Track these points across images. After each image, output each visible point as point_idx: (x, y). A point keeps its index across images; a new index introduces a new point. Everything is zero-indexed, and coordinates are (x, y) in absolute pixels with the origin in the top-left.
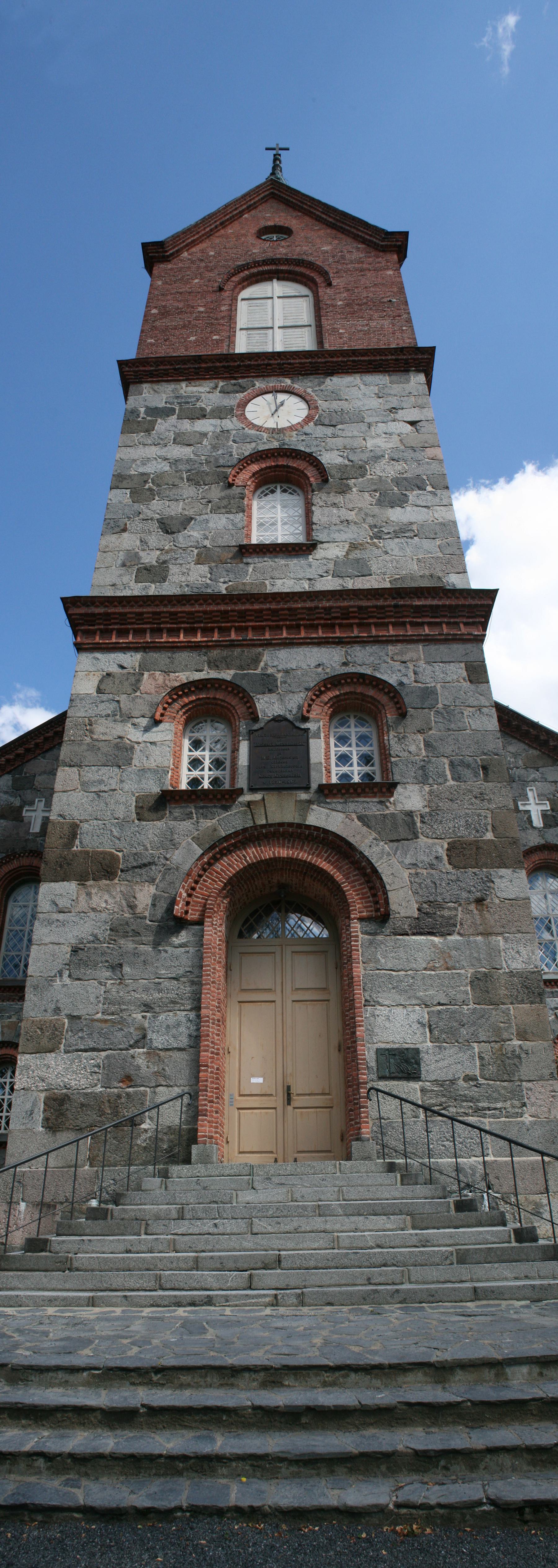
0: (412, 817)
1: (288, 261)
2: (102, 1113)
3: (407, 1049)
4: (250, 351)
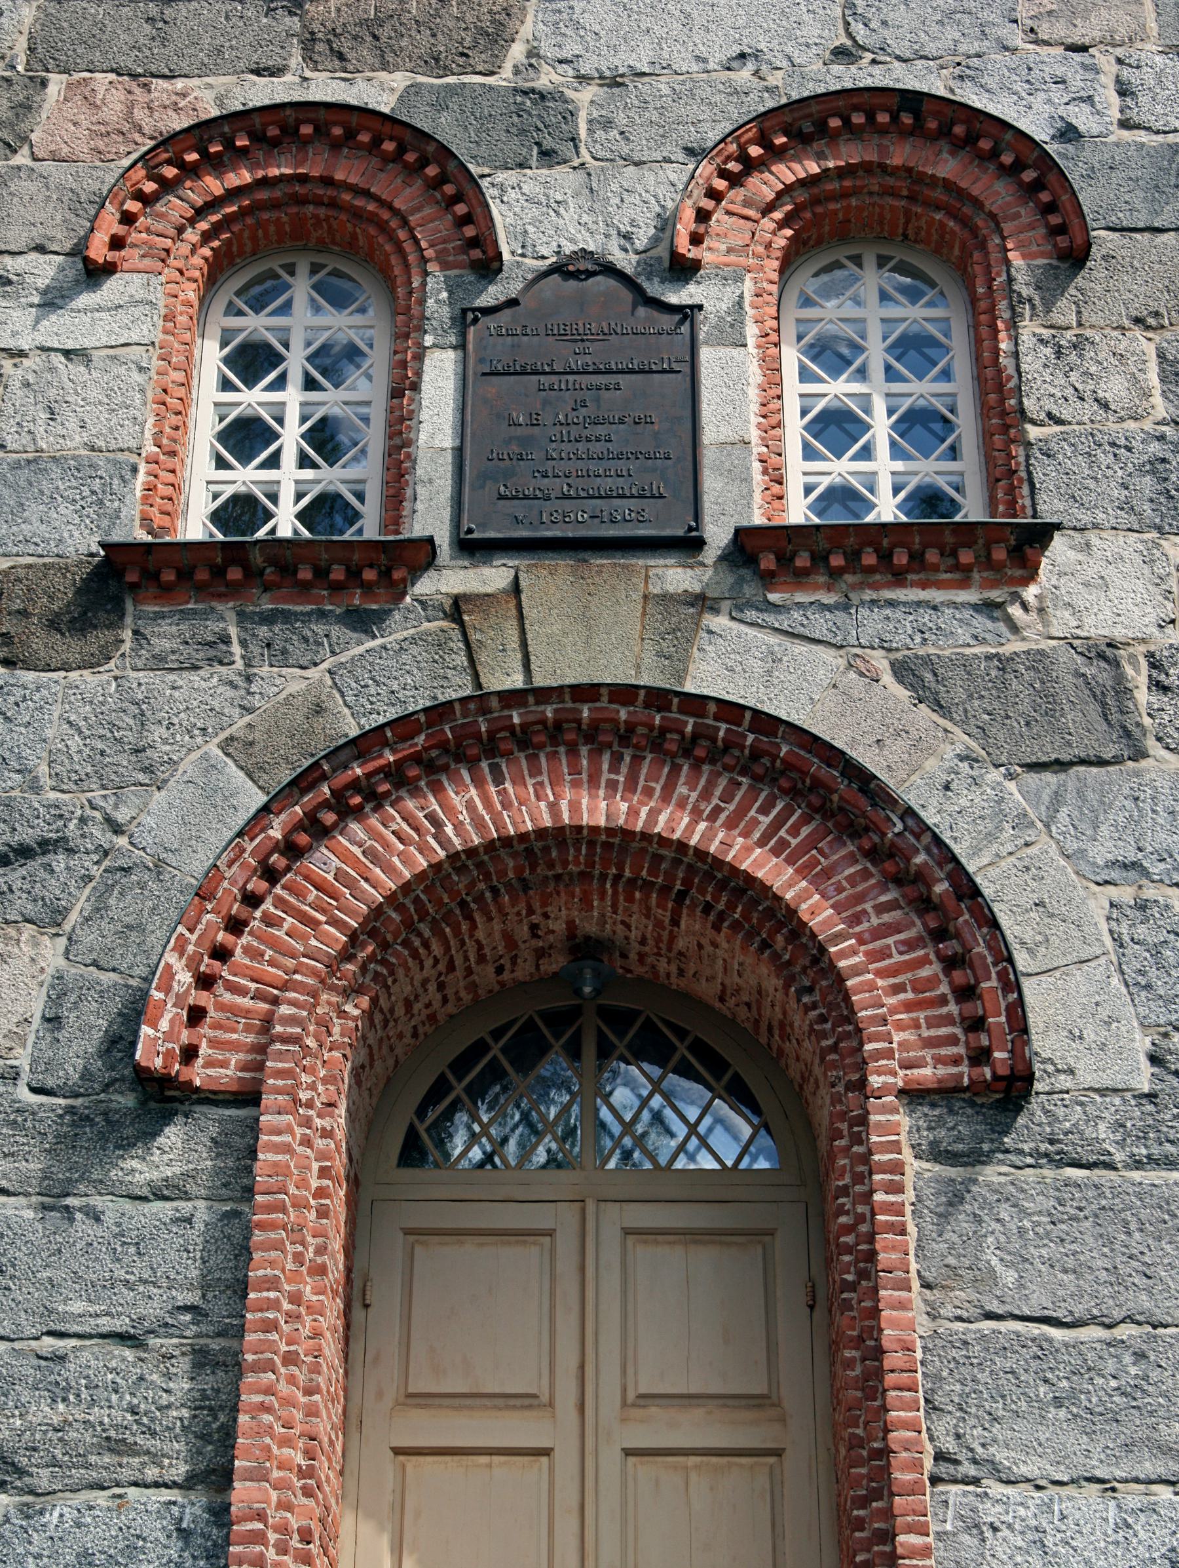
0: (1115, 663)
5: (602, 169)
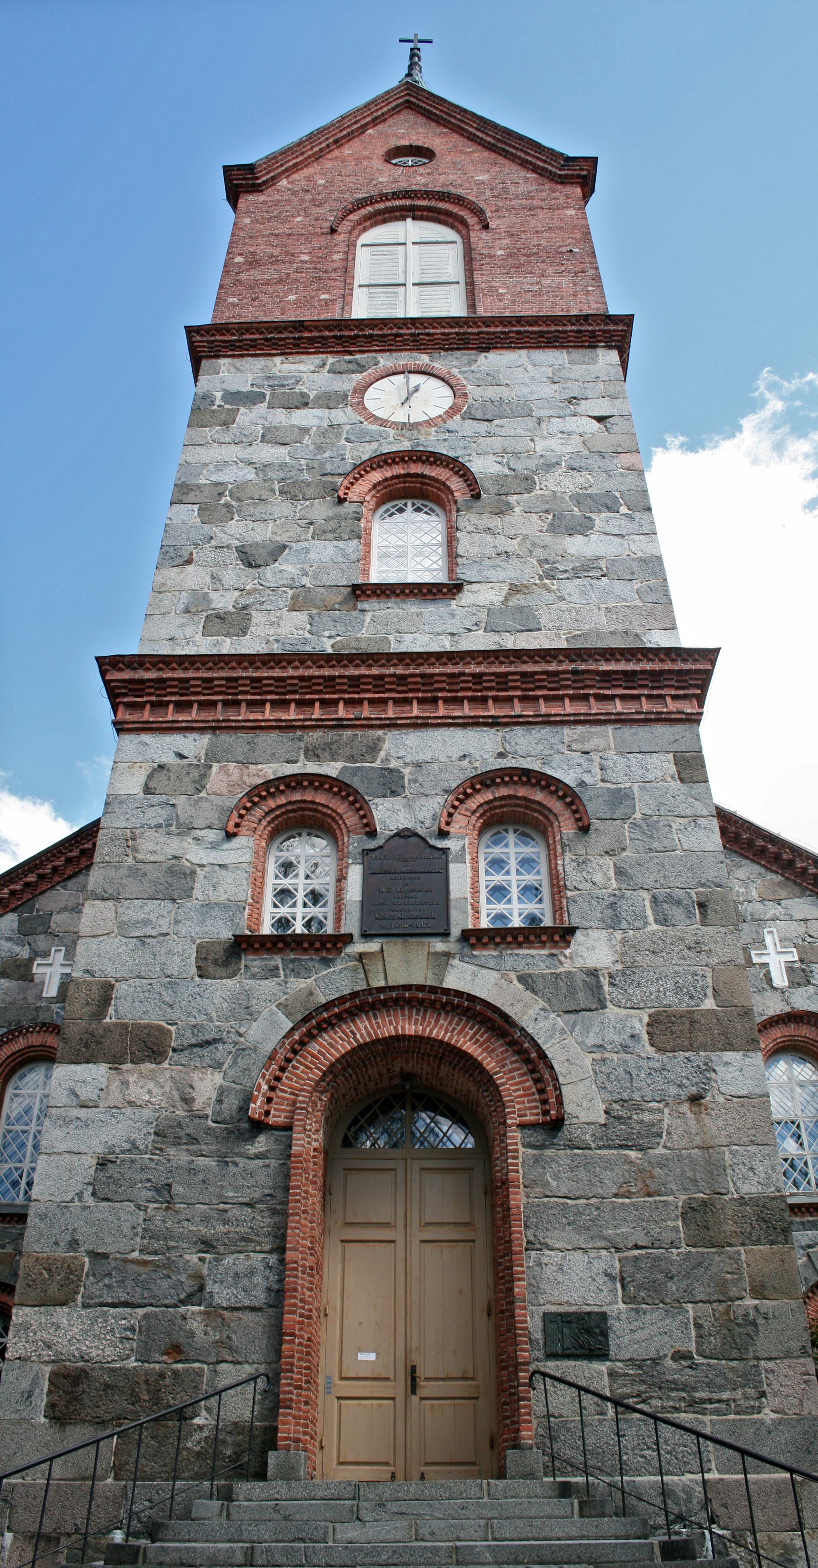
0: (597, 976)
1: (428, 194)
2: (135, 1400)
3: (589, 1313)
4: (372, 316)
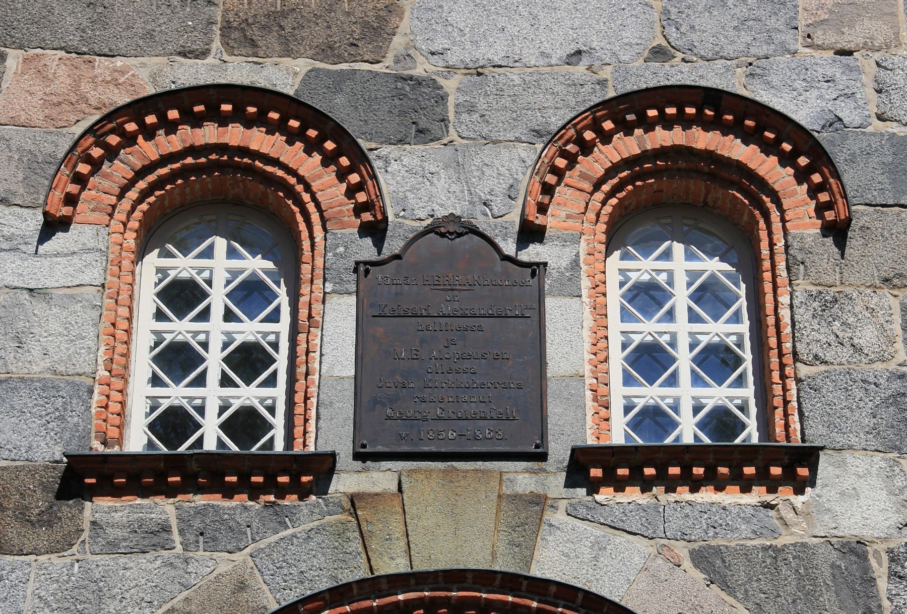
0: (863, 557)
5: (467, 146)
